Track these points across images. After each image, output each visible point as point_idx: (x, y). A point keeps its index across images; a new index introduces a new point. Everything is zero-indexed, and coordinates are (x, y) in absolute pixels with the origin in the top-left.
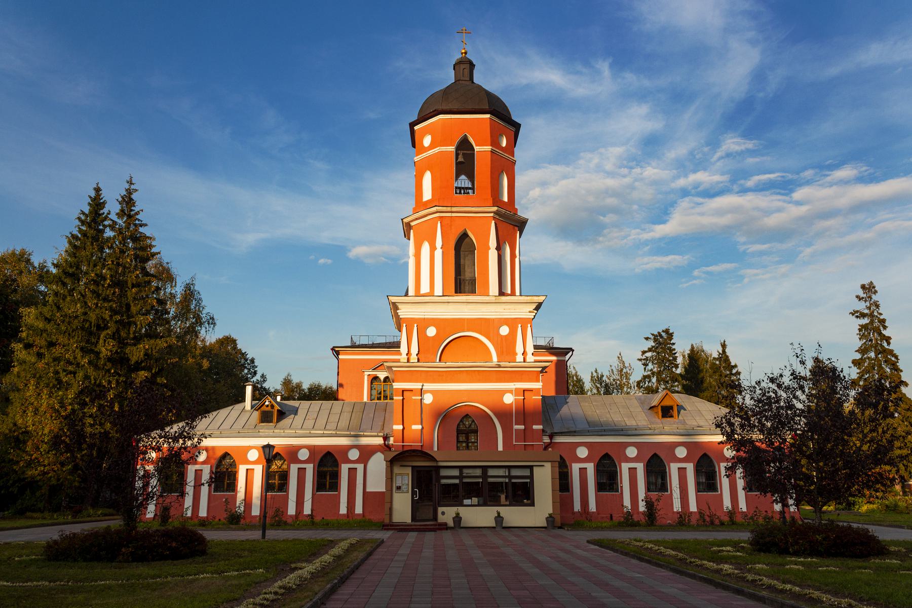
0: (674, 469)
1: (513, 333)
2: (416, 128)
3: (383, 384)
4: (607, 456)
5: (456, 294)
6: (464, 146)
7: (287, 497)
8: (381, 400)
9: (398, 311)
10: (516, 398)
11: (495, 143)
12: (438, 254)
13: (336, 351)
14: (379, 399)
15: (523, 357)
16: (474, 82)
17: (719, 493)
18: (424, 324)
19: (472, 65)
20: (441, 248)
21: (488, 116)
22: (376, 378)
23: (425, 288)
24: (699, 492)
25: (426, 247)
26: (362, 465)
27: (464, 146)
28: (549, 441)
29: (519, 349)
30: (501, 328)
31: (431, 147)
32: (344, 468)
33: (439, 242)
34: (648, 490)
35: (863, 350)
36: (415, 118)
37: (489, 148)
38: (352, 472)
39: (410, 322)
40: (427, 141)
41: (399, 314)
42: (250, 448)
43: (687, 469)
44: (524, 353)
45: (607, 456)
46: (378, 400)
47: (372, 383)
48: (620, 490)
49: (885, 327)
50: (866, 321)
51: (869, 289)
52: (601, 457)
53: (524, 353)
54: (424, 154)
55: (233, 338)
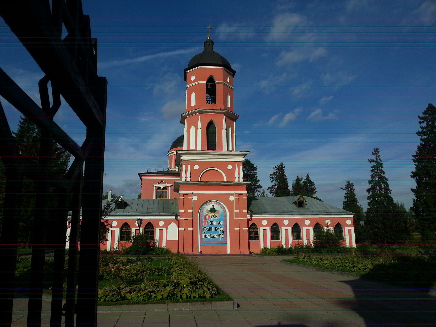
0: (283, 230)
1: (234, 169)
2: (187, 71)
3: (162, 191)
4: (275, 224)
5: (207, 150)
6: (211, 81)
7: (260, 242)
8: (161, 198)
9: (181, 157)
10: (235, 198)
11: (225, 80)
12: (199, 131)
13: (140, 175)
14: (160, 197)
15: (238, 179)
16: (214, 51)
17: (302, 240)
18: (193, 163)
19: (213, 43)
20: (201, 128)
21: (222, 67)
22: (159, 188)
23: (192, 147)
24: (293, 240)
25: (193, 128)
26: (165, 228)
27: (211, 81)
28: (250, 217)
29: (237, 175)
30: (229, 166)
31: (195, 81)
32: (157, 230)
33: (199, 126)
34: (293, 239)
35: (373, 177)
36: (187, 67)
37: (222, 82)
38: (161, 231)
39: (187, 162)
40: (193, 78)
41: (182, 159)
42: (160, 220)
43: (289, 230)
44: (239, 178)
45: (275, 224)
46: (160, 198)
47: (157, 190)
48: (281, 239)
49: (382, 167)
50: (374, 164)
51: (376, 151)
52: (251, 225)
53: (239, 178)
54: (192, 84)
55: (286, 179)
